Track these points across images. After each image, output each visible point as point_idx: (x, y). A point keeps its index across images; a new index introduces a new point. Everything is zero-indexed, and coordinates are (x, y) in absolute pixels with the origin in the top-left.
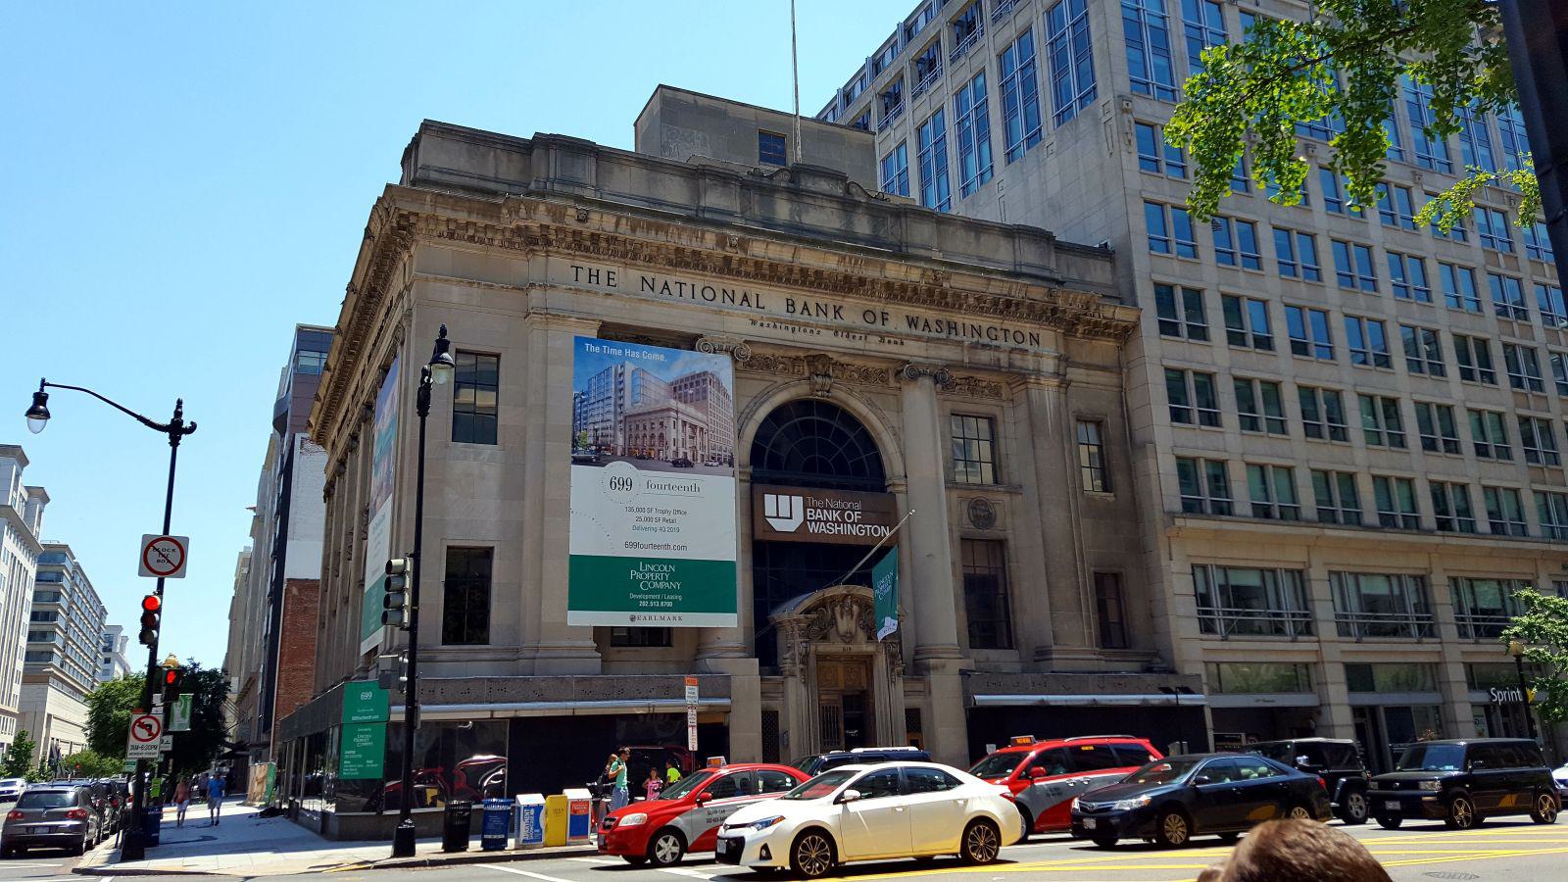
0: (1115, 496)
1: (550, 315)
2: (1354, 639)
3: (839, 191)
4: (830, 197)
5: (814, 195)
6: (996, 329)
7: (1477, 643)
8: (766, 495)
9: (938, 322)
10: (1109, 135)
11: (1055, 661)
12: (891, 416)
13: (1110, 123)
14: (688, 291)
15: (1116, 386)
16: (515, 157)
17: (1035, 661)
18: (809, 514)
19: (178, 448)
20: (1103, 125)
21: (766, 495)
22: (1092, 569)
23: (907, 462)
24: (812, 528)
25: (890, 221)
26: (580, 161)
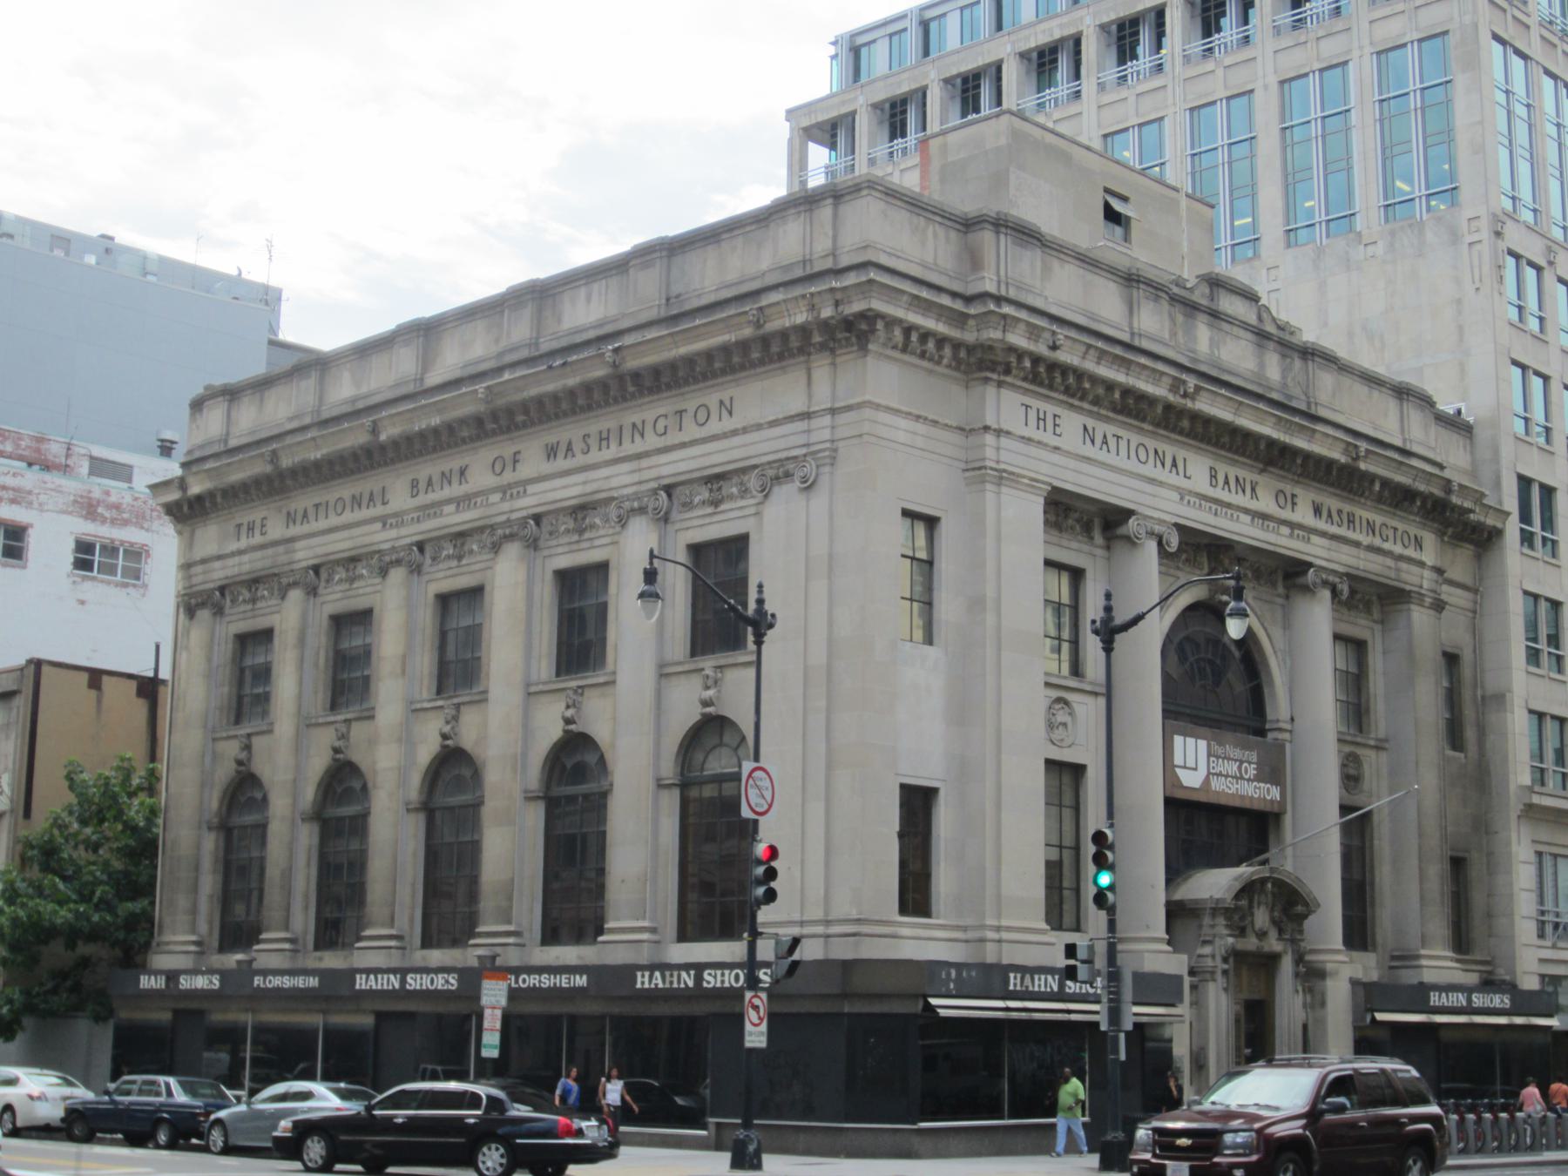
0: (1466, 757)
1: (1004, 477)
2: (1549, 944)
3: (1252, 319)
4: (1245, 326)
5: (1230, 320)
6: (1387, 527)
7: (1554, 947)
8: (1175, 736)
9: (1340, 512)
10: (1476, 263)
11: (1425, 970)
12: (1277, 633)
13: (1477, 247)
14: (1123, 444)
15: (1469, 610)
16: (953, 234)
17: (1392, 968)
18: (1212, 765)
19: (1113, 654)
20: (1466, 246)
21: (1175, 736)
22: (1449, 853)
23: (683, 677)
24: (1217, 785)
25: (1298, 363)
26: (1029, 253)
